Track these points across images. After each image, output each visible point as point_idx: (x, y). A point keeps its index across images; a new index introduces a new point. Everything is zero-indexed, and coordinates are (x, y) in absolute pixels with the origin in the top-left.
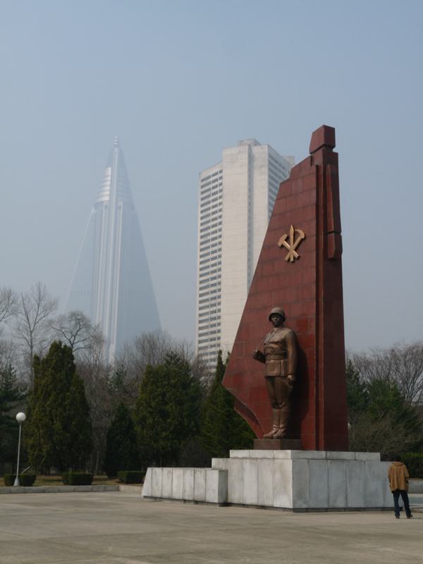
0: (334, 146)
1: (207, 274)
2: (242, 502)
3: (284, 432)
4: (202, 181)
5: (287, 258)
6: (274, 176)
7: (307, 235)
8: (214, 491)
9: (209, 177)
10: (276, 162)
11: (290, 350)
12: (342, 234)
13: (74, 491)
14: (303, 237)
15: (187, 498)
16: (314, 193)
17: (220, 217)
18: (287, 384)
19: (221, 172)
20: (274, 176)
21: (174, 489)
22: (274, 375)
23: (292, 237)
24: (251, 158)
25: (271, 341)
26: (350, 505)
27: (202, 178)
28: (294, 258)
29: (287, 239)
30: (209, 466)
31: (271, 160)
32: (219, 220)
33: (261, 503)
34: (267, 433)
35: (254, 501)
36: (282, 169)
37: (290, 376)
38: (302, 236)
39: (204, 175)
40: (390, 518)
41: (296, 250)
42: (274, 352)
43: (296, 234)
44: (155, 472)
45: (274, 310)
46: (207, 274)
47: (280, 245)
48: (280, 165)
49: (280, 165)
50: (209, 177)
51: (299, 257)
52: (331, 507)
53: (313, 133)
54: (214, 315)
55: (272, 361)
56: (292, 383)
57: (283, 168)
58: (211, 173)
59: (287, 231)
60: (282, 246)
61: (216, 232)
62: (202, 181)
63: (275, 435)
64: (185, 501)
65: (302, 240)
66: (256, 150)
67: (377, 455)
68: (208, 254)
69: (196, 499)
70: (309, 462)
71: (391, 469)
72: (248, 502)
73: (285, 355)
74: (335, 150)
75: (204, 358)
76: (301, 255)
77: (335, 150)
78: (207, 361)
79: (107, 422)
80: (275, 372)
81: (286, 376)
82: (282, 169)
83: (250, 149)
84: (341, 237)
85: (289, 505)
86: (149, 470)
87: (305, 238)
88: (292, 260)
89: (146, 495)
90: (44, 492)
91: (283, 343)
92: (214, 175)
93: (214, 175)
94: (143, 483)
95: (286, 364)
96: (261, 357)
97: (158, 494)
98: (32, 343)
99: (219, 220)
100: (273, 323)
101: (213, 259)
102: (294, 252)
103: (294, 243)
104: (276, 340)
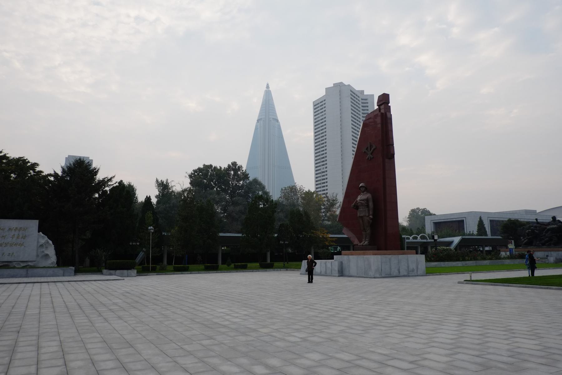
0: (389, 103)
3: (369, 242)
5: (367, 158)
6: (353, 102)
10: (355, 94)
11: (371, 204)
12: (394, 146)
14: (375, 148)
17: (325, 125)
19: (325, 100)
20: (353, 102)
22: (363, 216)
28: (371, 158)
31: (351, 100)
32: (324, 127)
38: (374, 147)
41: (371, 154)
47: (364, 152)
48: (357, 95)
49: (357, 95)
54: (324, 177)
61: (323, 133)
63: (364, 244)
65: (374, 149)
71: (377, 114)
73: (368, 206)
74: (389, 105)
75: (320, 193)
77: (389, 105)
78: (320, 195)
79: (223, 169)
84: (394, 147)
87: (376, 148)
88: (369, 159)
91: (367, 200)
92: (321, 102)
93: (321, 102)
99: (324, 127)
102: (371, 155)
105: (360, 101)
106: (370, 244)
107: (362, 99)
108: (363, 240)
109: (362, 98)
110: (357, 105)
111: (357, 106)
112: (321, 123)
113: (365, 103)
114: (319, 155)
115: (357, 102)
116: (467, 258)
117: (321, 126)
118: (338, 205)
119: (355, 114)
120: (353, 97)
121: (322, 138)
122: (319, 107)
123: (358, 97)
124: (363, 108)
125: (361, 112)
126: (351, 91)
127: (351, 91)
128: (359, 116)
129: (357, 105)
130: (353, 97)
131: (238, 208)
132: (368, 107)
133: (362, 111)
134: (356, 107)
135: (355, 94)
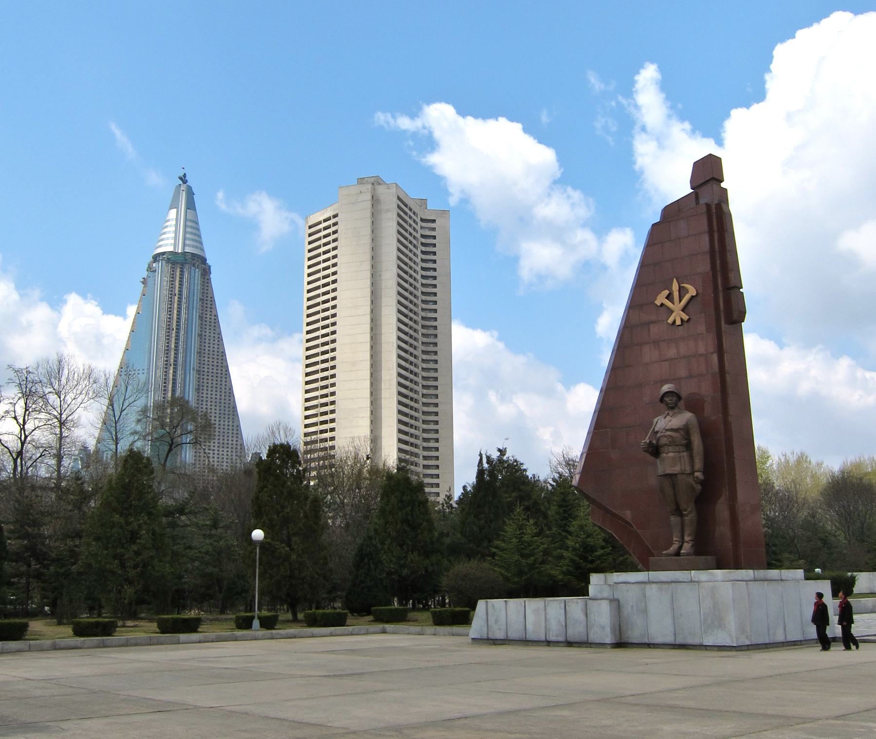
1: (317, 346)
2: (646, 641)
4: (310, 227)
5: (670, 321)
7: (699, 292)
8: (603, 628)
9: (319, 223)
10: (406, 206)
13: (331, 635)
14: (694, 295)
15: (531, 636)
16: (706, 238)
18: (693, 483)
19: (335, 216)
21: (530, 627)
23: (676, 294)
24: (375, 201)
25: (667, 427)
26: (790, 638)
27: (310, 224)
28: (682, 320)
29: (669, 297)
30: (582, 591)
33: (679, 641)
34: (667, 549)
35: (670, 639)
36: (412, 215)
37: (697, 474)
38: (692, 291)
39: (313, 220)
40: (815, 656)
41: (683, 310)
42: (673, 443)
43: (682, 291)
44: (493, 606)
45: (666, 388)
46: (317, 346)
48: (410, 210)
49: (410, 210)
50: (319, 223)
51: (689, 320)
52: (677, 643)
53: (695, 163)
55: (671, 454)
56: (702, 483)
57: (414, 213)
58: (321, 219)
59: (670, 288)
60: (662, 305)
62: (310, 227)
64: (548, 643)
66: (381, 189)
67: (800, 573)
68: (317, 321)
69: (570, 639)
70: (747, 584)
72: (659, 640)
73: (688, 446)
74: (723, 185)
76: (691, 317)
77: (723, 185)
80: (676, 469)
81: (693, 473)
82: (412, 215)
83: (374, 189)
85: (608, 640)
86: (481, 604)
88: (678, 322)
89: (478, 636)
90: (352, 634)
91: (686, 430)
92: (325, 221)
93: (325, 221)
94: (471, 624)
95: (691, 458)
96: (655, 450)
97: (499, 635)
98: (116, 436)
100: (667, 404)
101: (324, 327)
102: (682, 312)
103: (680, 301)
104: (675, 427)
105: (418, 282)
106: (132, 449)
107: (422, 220)
108: (675, 539)
109: (423, 218)
110: (412, 264)
111: (411, 268)
112: (324, 302)
113: (429, 294)
114: (315, 415)
115: (411, 234)
116: (65, 621)
117: (324, 294)
118: (309, 500)
119: (407, 235)
120: (402, 214)
121: (325, 374)
122: (319, 239)
123: (414, 213)
124: (424, 257)
125: (420, 299)
126: (399, 198)
127: (399, 198)
128: (414, 258)
129: (412, 264)
130: (402, 214)
131: (16, 547)
132: (434, 245)
133: (421, 339)
134: (410, 246)
135: (406, 206)
